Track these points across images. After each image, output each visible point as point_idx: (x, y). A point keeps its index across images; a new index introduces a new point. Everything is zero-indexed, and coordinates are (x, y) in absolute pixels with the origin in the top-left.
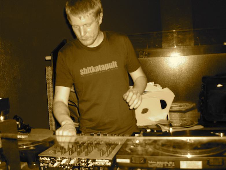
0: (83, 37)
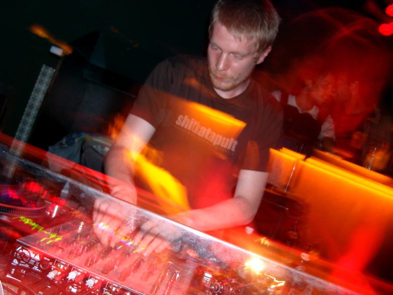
0: (219, 71)
